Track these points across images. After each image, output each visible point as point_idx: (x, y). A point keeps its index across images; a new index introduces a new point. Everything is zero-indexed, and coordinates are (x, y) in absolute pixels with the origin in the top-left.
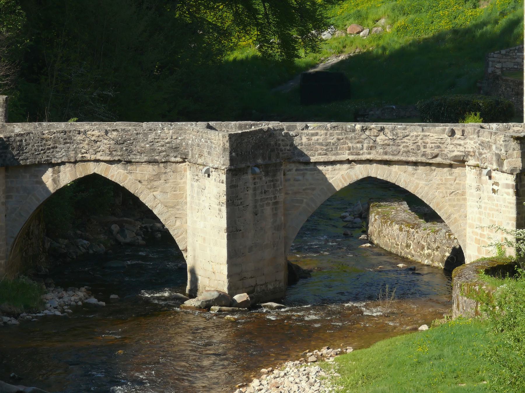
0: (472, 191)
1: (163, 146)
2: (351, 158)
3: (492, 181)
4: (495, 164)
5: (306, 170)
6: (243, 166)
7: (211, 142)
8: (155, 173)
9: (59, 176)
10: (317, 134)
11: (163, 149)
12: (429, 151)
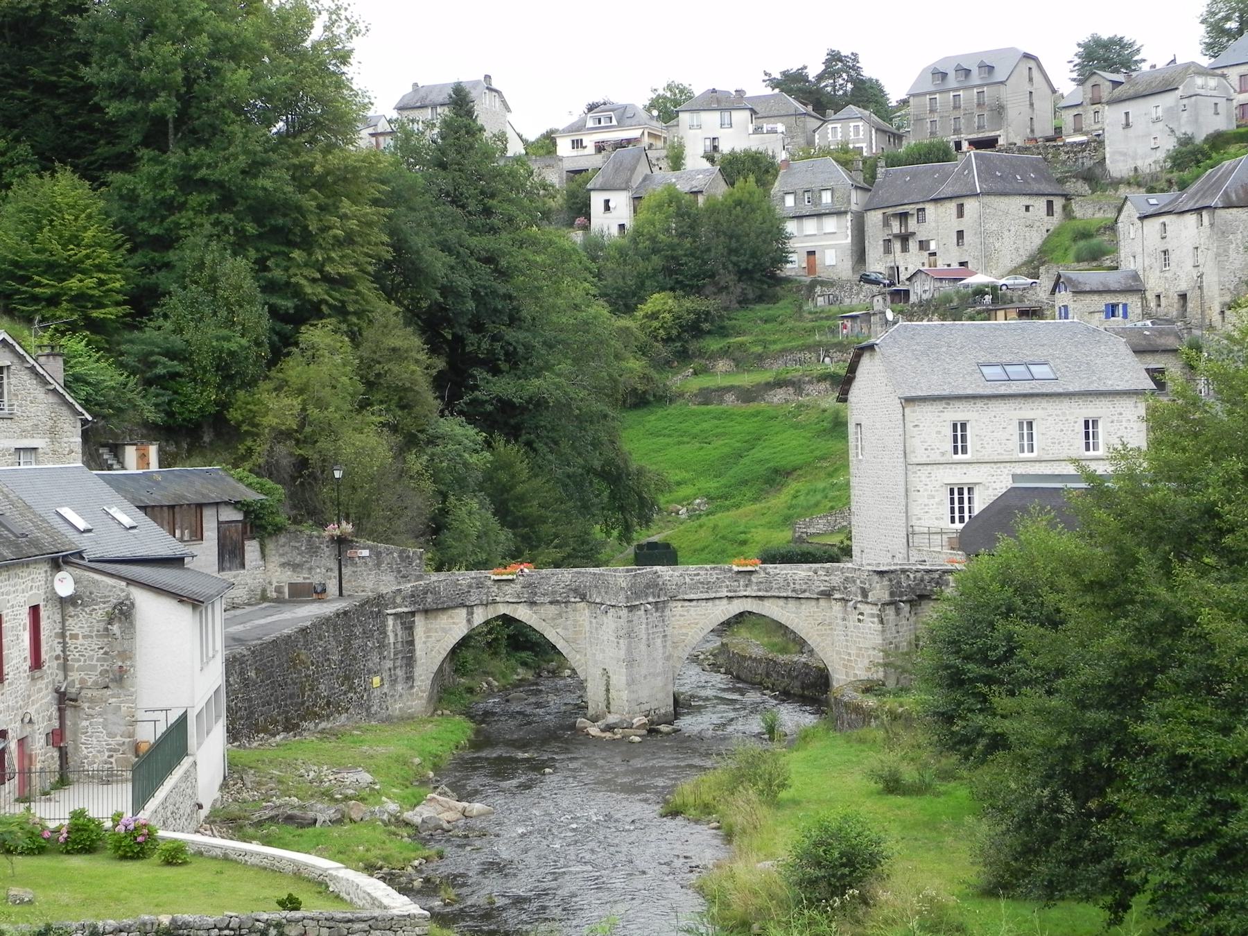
2: (730, 594)
10: (698, 574)
12: (797, 587)
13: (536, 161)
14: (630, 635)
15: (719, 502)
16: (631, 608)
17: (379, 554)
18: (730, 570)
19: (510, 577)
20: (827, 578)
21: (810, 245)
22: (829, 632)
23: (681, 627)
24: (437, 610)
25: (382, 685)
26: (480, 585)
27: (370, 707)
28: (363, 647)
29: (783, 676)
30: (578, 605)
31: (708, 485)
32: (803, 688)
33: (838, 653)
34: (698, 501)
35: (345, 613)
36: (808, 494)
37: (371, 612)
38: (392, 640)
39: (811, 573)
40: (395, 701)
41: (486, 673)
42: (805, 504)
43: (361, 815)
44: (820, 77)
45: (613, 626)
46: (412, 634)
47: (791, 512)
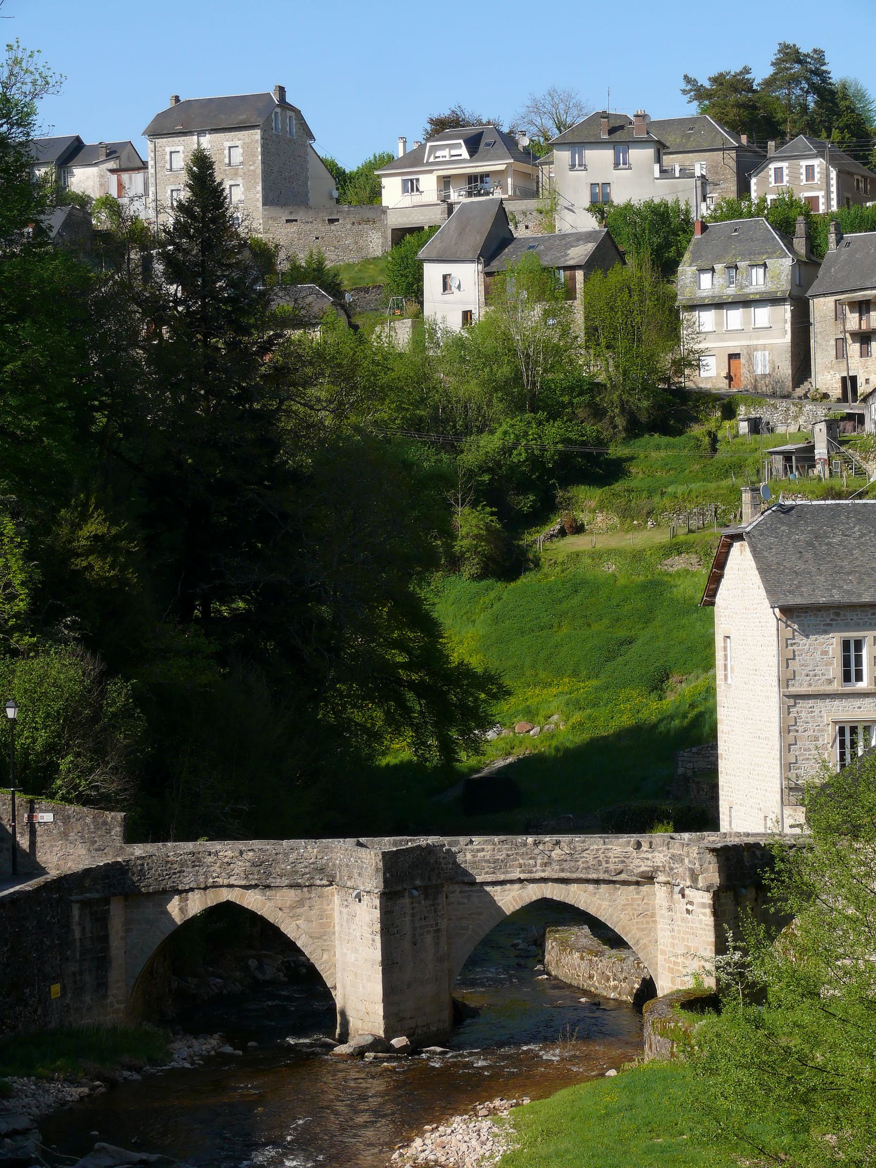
3: (685, 900)
6: (400, 888)
9: (186, 905)
10: (483, 850)
11: (307, 870)
12: (612, 867)
13: (349, 212)
17: (66, 820)
21: (734, 345)
38: (77, 935)
44: (769, 83)
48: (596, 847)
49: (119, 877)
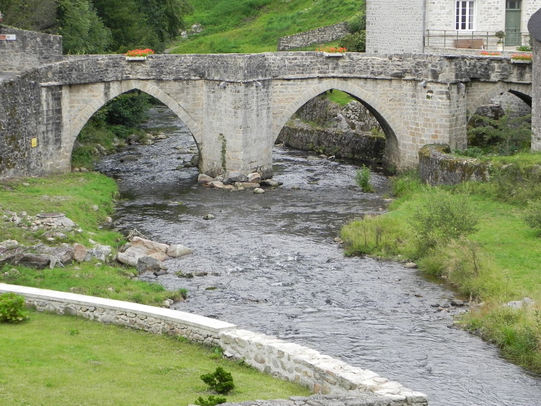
0: (408, 98)
1: (185, 68)
2: (321, 75)
3: (427, 90)
4: (430, 77)
5: (288, 84)
6: (251, 80)
7: (228, 64)
8: (179, 88)
9: (109, 91)
10: (296, 59)
11: (186, 70)
12: (375, 70)
14: (246, 106)
15: (210, 27)
16: (248, 84)
17: (24, 39)
18: (322, 55)
19: (142, 58)
20: (400, 63)
22: (398, 106)
23: (280, 101)
24: (80, 84)
25: (38, 145)
26: (116, 65)
27: (29, 163)
28: (24, 113)
29: (334, 144)
30: (197, 82)
31: (200, 15)
32: (353, 153)
33: (406, 123)
34: (194, 26)
35: (11, 83)
36: (280, 20)
37: (30, 84)
38: (45, 108)
39: (387, 59)
40: (47, 159)
41: (97, 141)
42: (279, 28)
43: (84, 256)
45: (231, 99)
46: (59, 104)
47: (268, 33)
48: (366, 58)
49: (68, 73)
